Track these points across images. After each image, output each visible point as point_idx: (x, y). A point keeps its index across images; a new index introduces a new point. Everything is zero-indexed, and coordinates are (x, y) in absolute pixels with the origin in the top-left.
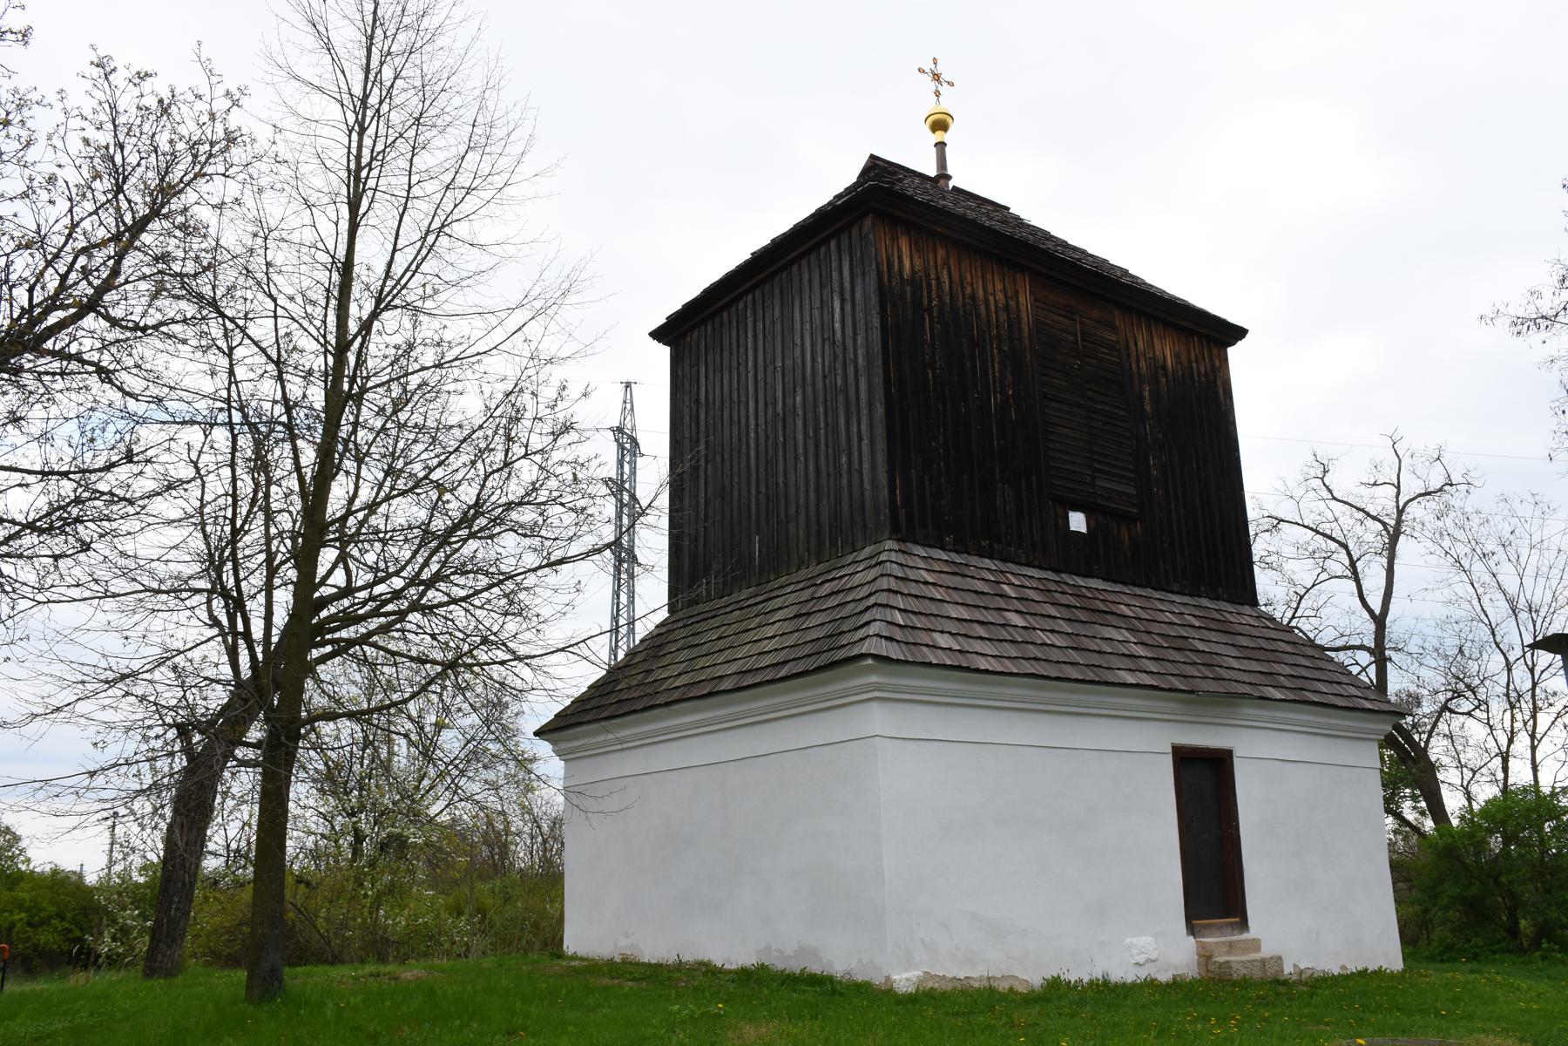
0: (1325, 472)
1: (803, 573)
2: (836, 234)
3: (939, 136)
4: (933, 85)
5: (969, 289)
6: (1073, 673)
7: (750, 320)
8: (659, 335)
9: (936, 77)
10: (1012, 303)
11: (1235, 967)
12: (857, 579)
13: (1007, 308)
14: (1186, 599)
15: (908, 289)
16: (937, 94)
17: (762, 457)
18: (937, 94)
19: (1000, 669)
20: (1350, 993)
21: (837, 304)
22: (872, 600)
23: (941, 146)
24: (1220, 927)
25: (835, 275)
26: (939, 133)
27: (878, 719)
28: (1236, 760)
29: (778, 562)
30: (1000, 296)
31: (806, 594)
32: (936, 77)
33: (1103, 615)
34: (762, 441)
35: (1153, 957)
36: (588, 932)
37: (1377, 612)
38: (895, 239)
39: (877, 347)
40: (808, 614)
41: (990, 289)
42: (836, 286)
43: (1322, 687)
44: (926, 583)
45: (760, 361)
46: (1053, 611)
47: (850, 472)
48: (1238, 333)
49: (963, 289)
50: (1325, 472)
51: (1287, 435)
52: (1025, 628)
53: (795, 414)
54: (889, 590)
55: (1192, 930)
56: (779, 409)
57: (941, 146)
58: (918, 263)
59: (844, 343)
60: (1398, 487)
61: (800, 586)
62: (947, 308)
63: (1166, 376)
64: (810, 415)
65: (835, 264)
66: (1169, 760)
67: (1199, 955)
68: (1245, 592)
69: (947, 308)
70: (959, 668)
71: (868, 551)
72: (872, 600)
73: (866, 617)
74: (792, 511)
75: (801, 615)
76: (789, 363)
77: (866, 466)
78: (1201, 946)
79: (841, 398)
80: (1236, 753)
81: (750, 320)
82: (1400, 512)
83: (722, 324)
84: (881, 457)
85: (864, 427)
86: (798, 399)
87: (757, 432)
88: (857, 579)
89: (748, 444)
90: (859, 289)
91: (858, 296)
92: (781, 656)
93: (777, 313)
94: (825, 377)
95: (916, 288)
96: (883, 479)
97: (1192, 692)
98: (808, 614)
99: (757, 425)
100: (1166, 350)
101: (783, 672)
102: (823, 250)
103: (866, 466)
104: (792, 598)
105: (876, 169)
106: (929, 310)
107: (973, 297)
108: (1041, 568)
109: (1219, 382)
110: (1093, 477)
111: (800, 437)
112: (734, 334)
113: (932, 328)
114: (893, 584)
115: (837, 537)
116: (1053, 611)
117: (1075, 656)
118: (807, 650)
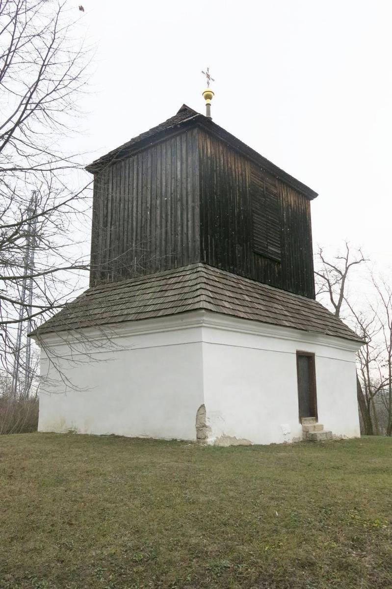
0: (321, 252)
1: (158, 274)
2: (180, 134)
3: (208, 101)
4: (207, 79)
5: (229, 165)
6: (268, 320)
7: (135, 166)
8: (89, 169)
9: (208, 76)
10: (244, 173)
11: (318, 435)
12: (187, 278)
13: (242, 174)
14: (294, 295)
15: (209, 161)
16: (208, 83)
17: (139, 225)
18: (208, 83)
19: (247, 317)
20: (341, 444)
21: (179, 164)
22: (198, 286)
23: (208, 105)
24: (310, 420)
25: (179, 152)
26: (209, 100)
27: (206, 335)
28: (315, 357)
29: (146, 268)
30: (240, 169)
31: (163, 282)
32: (208, 76)
33: (272, 299)
34: (140, 217)
35: (289, 432)
36: (48, 421)
37: (337, 304)
38: (205, 139)
39: (197, 183)
40: (166, 290)
41: (236, 166)
42: (179, 156)
43: (342, 331)
44: (216, 281)
45: (140, 184)
46: (257, 296)
47: (182, 234)
48: (313, 195)
49: (228, 165)
50: (321, 252)
51: (330, 235)
52: (250, 301)
53: (156, 208)
54: (205, 283)
55: (301, 422)
56: (149, 205)
57: (208, 105)
58: (213, 151)
59: (181, 180)
60: (347, 260)
61: (158, 279)
62: (222, 171)
63: (291, 209)
64: (163, 209)
65: (179, 147)
66: (295, 356)
67: (304, 431)
68: (313, 296)
69: (222, 171)
70: (234, 316)
71: (190, 266)
72: (198, 286)
73: (198, 293)
74: (153, 247)
75: (162, 291)
76: (154, 186)
77: (190, 232)
78: (304, 427)
79: (179, 203)
80: (316, 354)
81: (135, 166)
82: (347, 268)
83: (121, 167)
84: (197, 229)
85: (190, 216)
86: (158, 202)
87: (137, 214)
88: (187, 278)
89: (132, 218)
90: (190, 159)
91: (189, 161)
92: (157, 307)
93: (149, 165)
94: (172, 194)
95: (212, 162)
96: (198, 237)
97: (306, 330)
98: (166, 290)
99: (137, 211)
100: (292, 199)
101: (161, 313)
102: (173, 141)
103: (190, 232)
104: (156, 283)
105: (185, 110)
106: (216, 171)
107: (231, 168)
108: (250, 279)
109: (307, 213)
110: (267, 245)
111: (158, 218)
112: (127, 172)
113: (217, 178)
114: (205, 280)
115: (175, 260)
116: (257, 296)
117: (269, 314)
118: (171, 305)
